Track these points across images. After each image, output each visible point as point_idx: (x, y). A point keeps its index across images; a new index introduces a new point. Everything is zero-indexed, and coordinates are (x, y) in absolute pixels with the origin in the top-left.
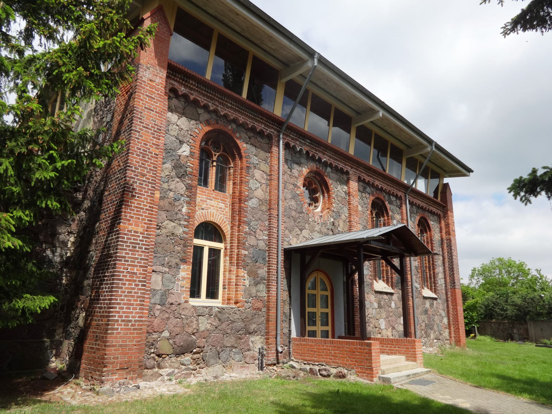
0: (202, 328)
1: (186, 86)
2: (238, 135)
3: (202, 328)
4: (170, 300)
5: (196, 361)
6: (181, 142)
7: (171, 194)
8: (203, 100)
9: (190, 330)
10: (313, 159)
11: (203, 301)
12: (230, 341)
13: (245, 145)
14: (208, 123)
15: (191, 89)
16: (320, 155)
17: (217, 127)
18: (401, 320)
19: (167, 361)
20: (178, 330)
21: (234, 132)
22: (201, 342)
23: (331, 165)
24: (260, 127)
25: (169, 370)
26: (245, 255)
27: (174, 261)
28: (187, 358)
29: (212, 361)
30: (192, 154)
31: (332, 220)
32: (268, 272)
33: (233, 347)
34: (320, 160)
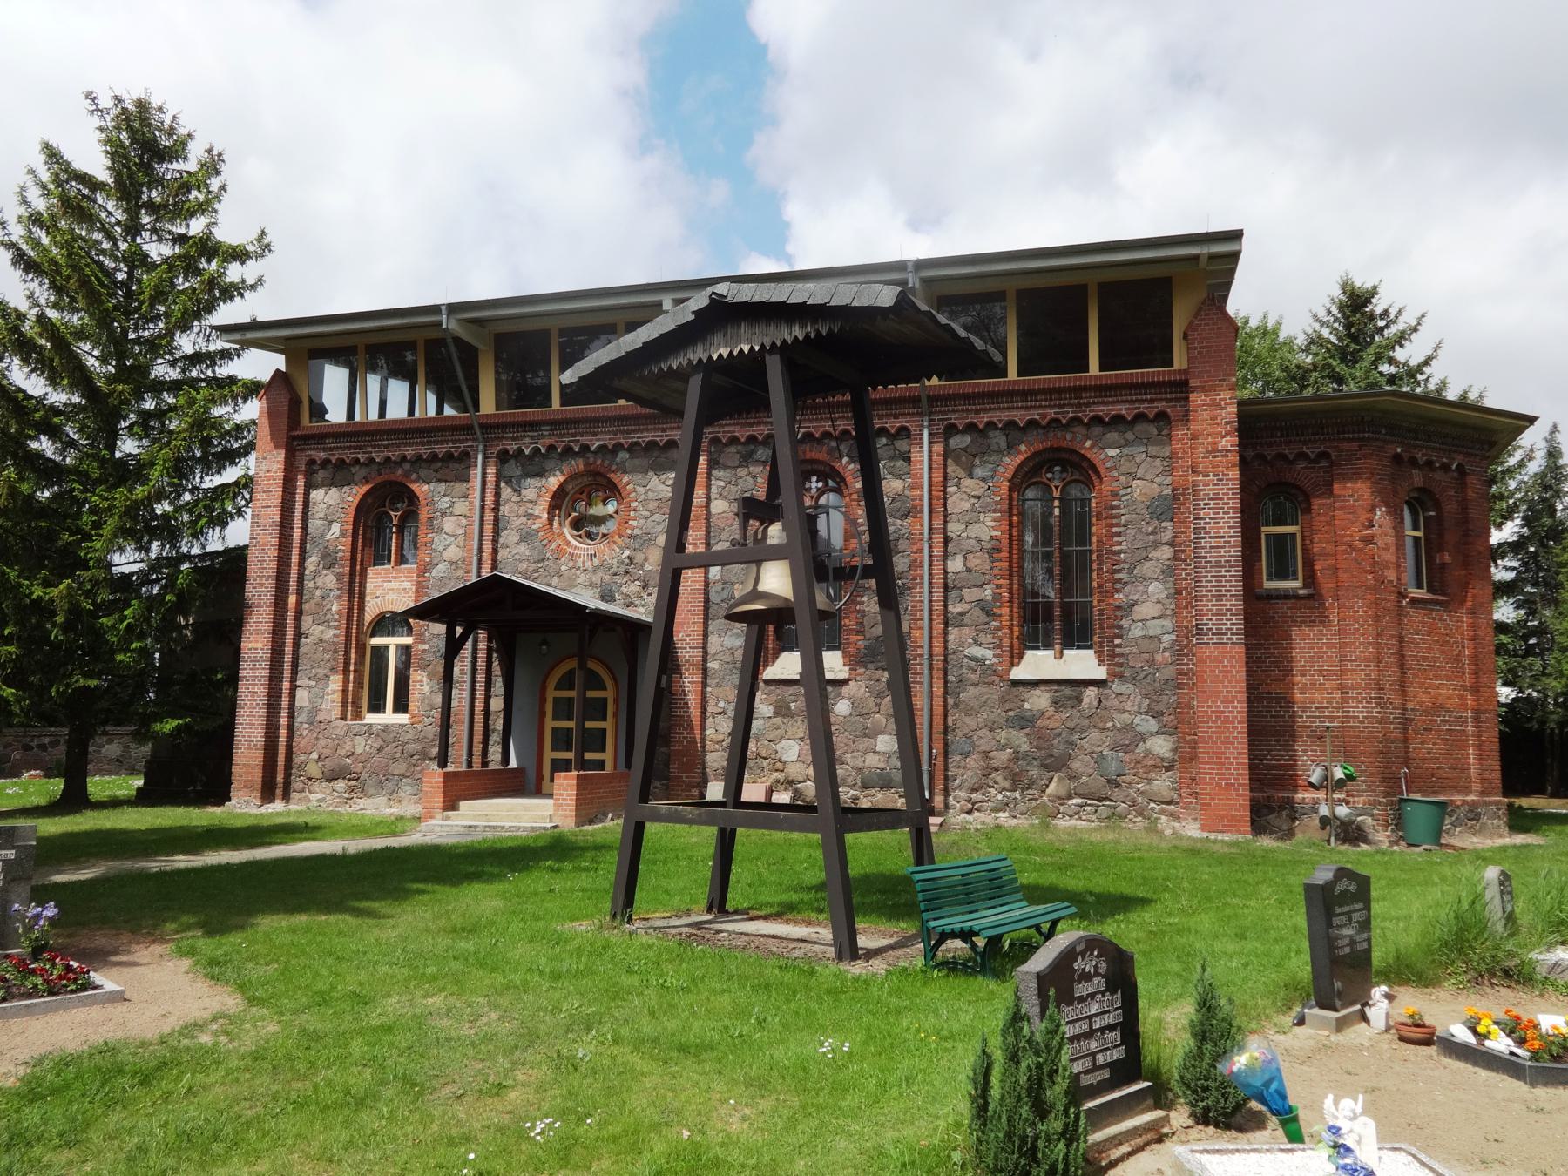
0: (359, 750)
1: (324, 450)
2: (414, 476)
3: (359, 750)
4: (319, 718)
5: (351, 789)
6: (331, 523)
7: (318, 592)
8: (348, 456)
9: (343, 752)
10: (568, 452)
11: (389, 717)
12: (399, 768)
13: (426, 487)
14: (366, 480)
15: (331, 449)
16: (585, 439)
17: (379, 480)
18: (756, 725)
19: (316, 786)
20: (327, 752)
21: (407, 475)
22: (358, 767)
23: (618, 447)
24: (441, 450)
25: (319, 796)
26: (424, 651)
27: (322, 672)
28: (341, 785)
29: (372, 791)
30: (343, 534)
31: (627, 553)
32: (946, 634)
33: (403, 776)
34: (585, 448)
